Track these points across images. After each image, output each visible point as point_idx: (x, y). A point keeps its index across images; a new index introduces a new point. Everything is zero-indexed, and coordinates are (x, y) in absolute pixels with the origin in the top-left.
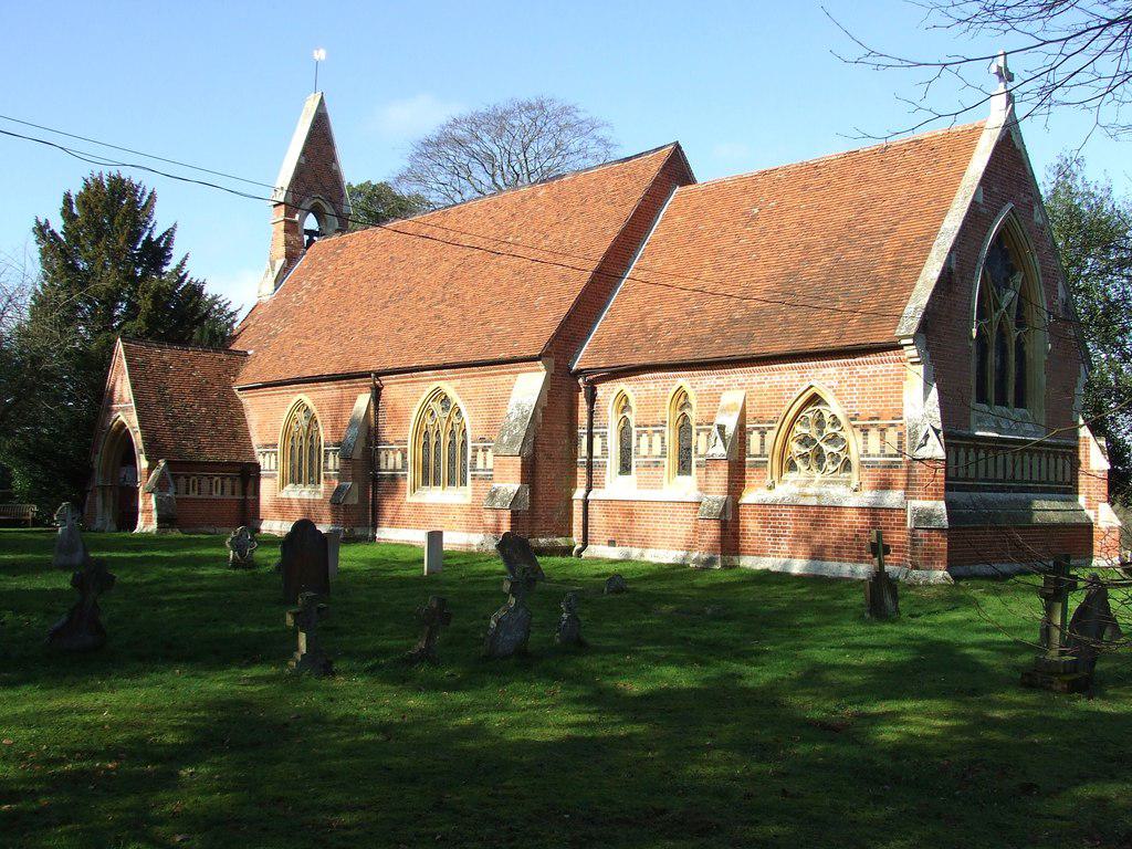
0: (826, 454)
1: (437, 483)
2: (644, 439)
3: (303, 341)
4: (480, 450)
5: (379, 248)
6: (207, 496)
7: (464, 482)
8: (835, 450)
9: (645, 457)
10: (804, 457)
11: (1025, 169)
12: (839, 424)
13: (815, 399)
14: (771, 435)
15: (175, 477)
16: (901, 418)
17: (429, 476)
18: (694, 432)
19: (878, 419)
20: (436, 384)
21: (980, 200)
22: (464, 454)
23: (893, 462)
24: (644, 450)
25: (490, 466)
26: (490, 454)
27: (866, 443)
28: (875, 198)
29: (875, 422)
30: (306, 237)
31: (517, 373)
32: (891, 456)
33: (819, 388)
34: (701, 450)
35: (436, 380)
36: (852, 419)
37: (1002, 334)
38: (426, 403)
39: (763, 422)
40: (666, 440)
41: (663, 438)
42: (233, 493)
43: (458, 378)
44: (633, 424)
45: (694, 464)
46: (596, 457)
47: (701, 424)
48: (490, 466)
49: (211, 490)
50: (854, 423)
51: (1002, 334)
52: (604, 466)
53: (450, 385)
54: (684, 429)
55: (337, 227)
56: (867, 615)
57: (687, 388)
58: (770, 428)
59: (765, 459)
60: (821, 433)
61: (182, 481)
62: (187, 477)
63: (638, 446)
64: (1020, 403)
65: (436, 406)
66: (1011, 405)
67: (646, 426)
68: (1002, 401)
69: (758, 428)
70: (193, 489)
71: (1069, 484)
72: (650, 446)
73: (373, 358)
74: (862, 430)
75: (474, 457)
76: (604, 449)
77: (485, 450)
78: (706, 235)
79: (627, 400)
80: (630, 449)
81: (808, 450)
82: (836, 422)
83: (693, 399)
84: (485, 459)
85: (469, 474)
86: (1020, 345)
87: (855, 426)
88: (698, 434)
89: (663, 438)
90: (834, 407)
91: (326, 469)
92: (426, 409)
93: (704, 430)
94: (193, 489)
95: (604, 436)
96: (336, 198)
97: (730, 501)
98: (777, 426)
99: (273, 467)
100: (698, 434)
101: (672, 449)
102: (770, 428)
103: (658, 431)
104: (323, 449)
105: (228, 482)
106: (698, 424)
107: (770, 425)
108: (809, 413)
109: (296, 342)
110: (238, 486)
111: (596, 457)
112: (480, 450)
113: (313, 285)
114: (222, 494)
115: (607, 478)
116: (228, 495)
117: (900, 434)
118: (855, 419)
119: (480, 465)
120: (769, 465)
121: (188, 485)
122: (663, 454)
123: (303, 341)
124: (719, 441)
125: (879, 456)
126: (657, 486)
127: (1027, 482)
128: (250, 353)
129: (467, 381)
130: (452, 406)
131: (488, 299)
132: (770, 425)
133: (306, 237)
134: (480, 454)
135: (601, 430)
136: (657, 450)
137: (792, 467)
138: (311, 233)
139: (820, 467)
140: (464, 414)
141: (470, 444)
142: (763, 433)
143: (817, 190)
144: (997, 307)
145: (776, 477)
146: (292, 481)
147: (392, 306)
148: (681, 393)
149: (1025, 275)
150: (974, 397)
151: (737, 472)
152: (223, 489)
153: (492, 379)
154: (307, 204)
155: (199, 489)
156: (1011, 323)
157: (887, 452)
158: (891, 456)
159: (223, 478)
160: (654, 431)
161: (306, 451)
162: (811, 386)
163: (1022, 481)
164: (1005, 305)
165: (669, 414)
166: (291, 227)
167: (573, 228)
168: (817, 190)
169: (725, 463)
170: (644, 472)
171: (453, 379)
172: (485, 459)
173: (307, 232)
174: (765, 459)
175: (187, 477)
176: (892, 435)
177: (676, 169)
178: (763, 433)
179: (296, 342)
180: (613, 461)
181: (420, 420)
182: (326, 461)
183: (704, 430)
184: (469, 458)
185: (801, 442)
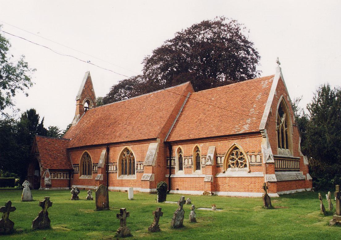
0: (239, 163)
1: (126, 174)
2: (186, 160)
3: (86, 136)
4: (139, 165)
5: (106, 111)
6: (66, 179)
7: (91, 174)
8: (242, 162)
9: (187, 165)
10: (233, 164)
11: (285, 87)
12: (243, 154)
13: (236, 148)
14: (223, 158)
15: (51, 174)
16: (261, 152)
17: (124, 172)
18: (201, 158)
19: (254, 152)
20: (125, 147)
21: (276, 94)
22: (134, 166)
23: (259, 164)
24: (186, 163)
25: (97, 170)
26: (142, 165)
27: (251, 159)
28: (246, 95)
29: (254, 153)
30: (85, 109)
31: (150, 143)
32: (259, 162)
33: (237, 145)
34: (203, 163)
35: (126, 145)
36: (247, 153)
37: (282, 130)
38: (122, 152)
39: (221, 155)
40: (193, 160)
41: (192, 160)
42: (66, 178)
43: (132, 145)
44: (183, 157)
45: (201, 167)
46: (172, 166)
47: (203, 156)
48: (97, 170)
49: (60, 177)
50: (247, 154)
51: (282, 130)
52: (174, 168)
53: (130, 147)
54: (198, 158)
55: (93, 106)
56: (264, 207)
57: (198, 146)
58: (223, 156)
59: (222, 165)
60: (237, 157)
61: (53, 174)
62: (60, 174)
63: (185, 162)
64: (287, 148)
65: (125, 153)
66: (285, 148)
67: (187, 157)
68: (283, 147)
69: (219, 156)
70: (62, 177)
71: (299, 169)
72: (188, 162)
73: (106, 140)
74: (250, 156)
75: (137, 167)
76: (174, 163)
77: (140, 164)
78: (200, 105)
79: (181, 150)
80: (182, 163)
81: (234, 162)
82: (241, 154)
83: (200, 149)
84: (140, 167)
85: (136, 171)
86: (286, 132)
87: (248, 155)
88: (202, 159)
89: (192, 160)
90: (241, 149)
91: (93, 171)
92: (123, 154)
93: (204, 157)
94: (62, 177)
95: (174, 160)
96: (93, 98)
97: (213, 176)
98: (225, 155)
99: (78, 170)
100: (202, 159)
101: (194, 163)
102: (223, 156)
103: (190, 158)
104: (92, 165)
105: (65, 175)
106: (202, 156)
107: (223, 155)
108: (234, 152)
109: (84, 136)
110: (68, 176)
111: (172, 166)
112: (139, 165)
113: (87, 121)
114: (64, 178)
115: (176, 171)
116: (65, 178)
117: (261, 156)
118: (248, 153)
119: (139, 169)
120: (223, 166)
121: (54, 176)
122: (192, 164)
123: (86, 136)
124: (209, 160)
125: (255, 163)
126: (190, 173)
127: (284, 168)
128: (71, 139)
129: (135, 146)
130: (130, 153)
131: (140, 123)
132: (223, 155)
133: (85, 109)
134: (139, 166)
135: (173, 158)
136: (190, 163)
137: (229, 166)
138: (86, 108)
139: (238, 167)
140: (134, 154)
141: (136, 163)
142: (221, 158)
143: (230, 93)
144: (281, 122)
145: (225, 170)
146: (83, 174)
147: (111, 126)
148: (197, 147)
149: (286, 114)
150: (278, 147)
151: (216, 168)
152: (64, 177)
153: (142, 145)
154: (85, 100)
155: (57, 177)
156: (284, 125)
157: (257, 161)
158: (259, 162)
159: (64, 174)
160: (189, 158)
161: (87, 165)
162: (235, 144)
163: (289, 168)
164: (282, 122)
165: (192, 152)
166: (81, 106)
167: (162, 104)
168: (230, 93)
169: (211, 167)
170: (187, 169)
171: (131, 145)
172: (140, 167)
173: (85, 107)
174: (222, 165)
175: (54, 174)
176: (258, 157)
177: (280, 64)
178: (221, 158)
179: (84, 136)
180: (177, 167)
181: (121, 156)
182: (93, 168)
183: (204, 157)
184: (136, 167)
185: (231, 160)
